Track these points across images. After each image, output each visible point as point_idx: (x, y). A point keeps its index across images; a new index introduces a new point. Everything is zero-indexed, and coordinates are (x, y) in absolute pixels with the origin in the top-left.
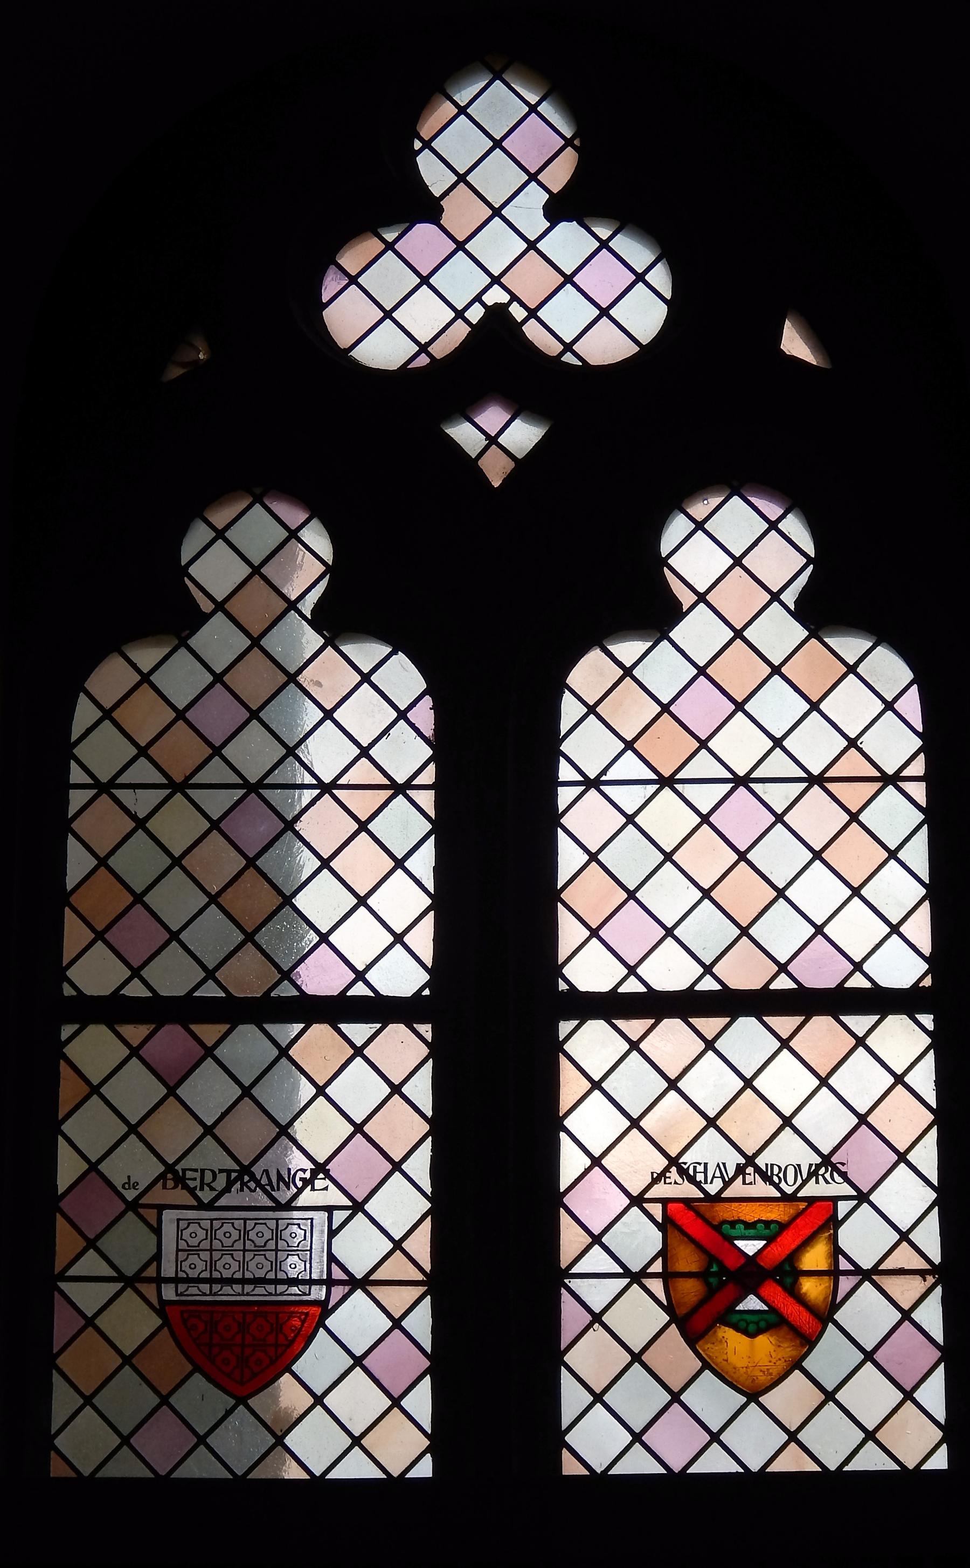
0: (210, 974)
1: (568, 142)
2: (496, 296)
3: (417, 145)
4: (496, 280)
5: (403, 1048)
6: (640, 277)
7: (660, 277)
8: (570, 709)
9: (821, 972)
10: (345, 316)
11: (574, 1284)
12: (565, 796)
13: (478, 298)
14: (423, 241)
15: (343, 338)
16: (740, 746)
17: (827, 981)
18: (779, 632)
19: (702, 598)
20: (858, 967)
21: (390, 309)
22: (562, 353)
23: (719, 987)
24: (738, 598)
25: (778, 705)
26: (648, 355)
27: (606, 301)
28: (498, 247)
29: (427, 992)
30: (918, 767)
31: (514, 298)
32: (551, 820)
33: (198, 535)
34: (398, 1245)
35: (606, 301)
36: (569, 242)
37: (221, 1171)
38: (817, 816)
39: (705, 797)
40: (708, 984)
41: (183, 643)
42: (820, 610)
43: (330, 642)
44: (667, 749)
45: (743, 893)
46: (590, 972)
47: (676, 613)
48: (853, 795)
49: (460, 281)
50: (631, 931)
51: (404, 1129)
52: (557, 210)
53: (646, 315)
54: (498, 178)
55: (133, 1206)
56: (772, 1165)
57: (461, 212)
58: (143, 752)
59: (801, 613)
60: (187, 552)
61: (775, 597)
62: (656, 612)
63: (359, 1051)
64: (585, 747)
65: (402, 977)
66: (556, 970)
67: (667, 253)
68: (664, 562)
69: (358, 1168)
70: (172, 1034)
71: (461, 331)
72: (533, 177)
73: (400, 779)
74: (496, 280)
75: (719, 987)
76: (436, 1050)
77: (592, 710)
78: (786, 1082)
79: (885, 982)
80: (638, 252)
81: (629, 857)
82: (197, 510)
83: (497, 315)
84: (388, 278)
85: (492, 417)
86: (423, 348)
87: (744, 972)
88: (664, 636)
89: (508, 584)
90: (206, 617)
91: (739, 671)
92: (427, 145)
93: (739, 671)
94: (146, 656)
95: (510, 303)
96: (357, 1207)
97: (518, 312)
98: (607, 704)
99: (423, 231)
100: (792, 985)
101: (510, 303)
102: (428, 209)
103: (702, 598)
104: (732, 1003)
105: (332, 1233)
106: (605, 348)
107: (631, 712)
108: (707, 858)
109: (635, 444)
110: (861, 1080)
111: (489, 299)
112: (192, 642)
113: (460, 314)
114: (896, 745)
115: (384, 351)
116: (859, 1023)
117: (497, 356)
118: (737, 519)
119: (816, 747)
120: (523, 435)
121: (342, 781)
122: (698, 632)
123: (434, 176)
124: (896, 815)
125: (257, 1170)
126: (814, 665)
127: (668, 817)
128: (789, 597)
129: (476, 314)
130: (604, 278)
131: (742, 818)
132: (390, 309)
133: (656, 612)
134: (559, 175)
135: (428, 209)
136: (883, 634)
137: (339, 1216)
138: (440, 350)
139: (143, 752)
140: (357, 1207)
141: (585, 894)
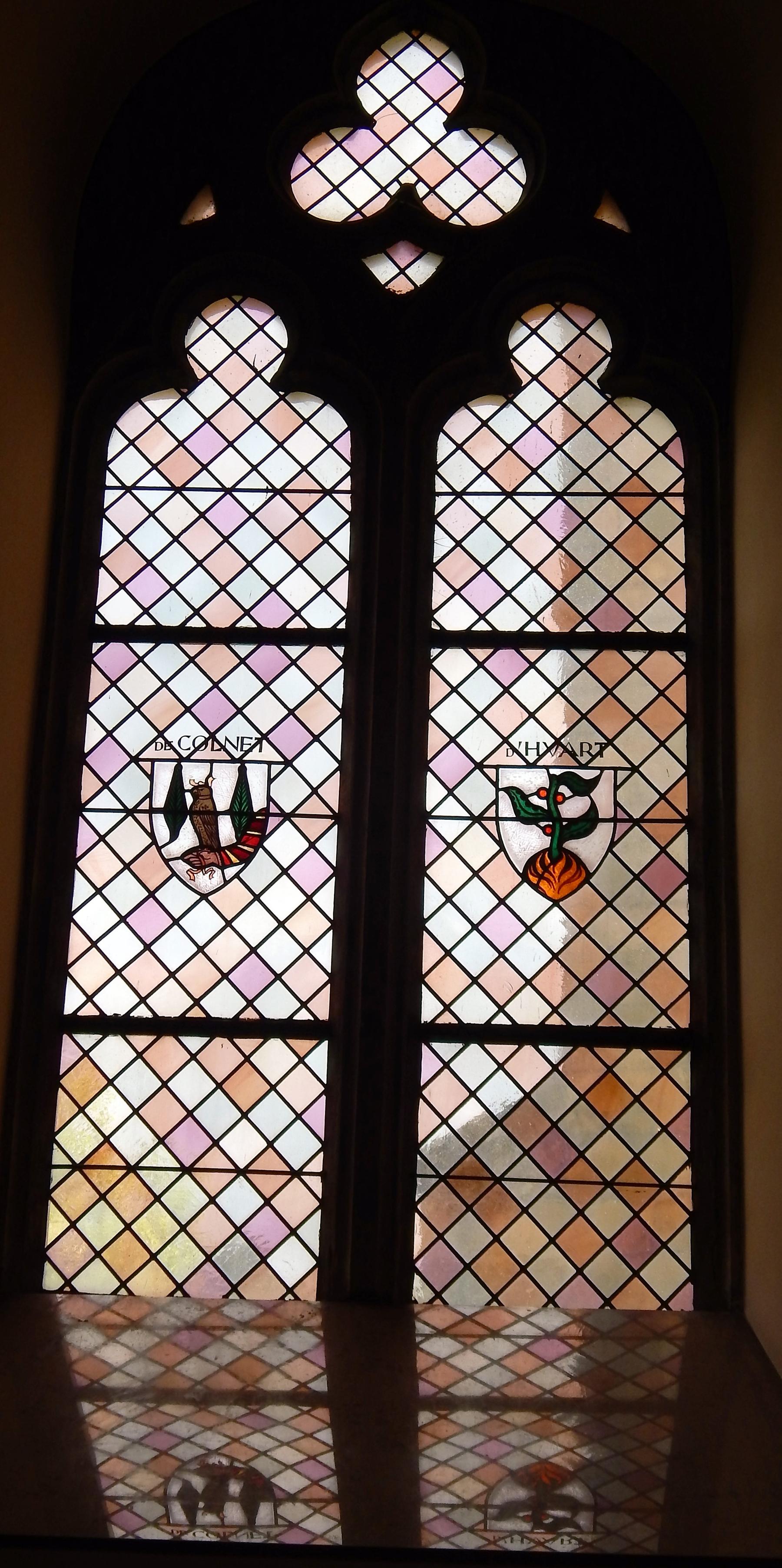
0: (197, 612)
1: (460, 82)
2: (409, 178)
3: (360, 80)
4: (409, 167)
5: (324, 661)
6: (505, 169)
7: (519, 170)
8: (444, 447)
9: (271, 616)
10: (306, 189)
11: (87, 814)
12: (110, 496)
13: (396, 179)
14: (363, 142)
15: (304, 204)
16: (229, 468)
17: (615, 627)
18: (260, 396)
19: (210, 374)
20: (298, 613)
21: (334, 184)
22: (450, 217)
23: (204, 625)
24: (234, 374)
25: (256, 444)
26: (508, 221)
27: (482, 184)
28: (411, 146)
29: (342, 626)
30: (347, 485)
31: (420, 179)
32: (100, 513)
33: (199, 327)
34: (315, 791)
35: (482, 184)
36: (459, 145)
37: (596, 744)
38: (279, 514)
39: (203, 501)
40: (482, 626)
41: (184, 397)
42: (285, 384)
43: (610, 402)
44: (180, 469)
45: (225, 564)
46: (453, 617)
47: (196, 383)
48: (302, 501)
49: (385, 168)
50: (483, 592)
51: (324, 714)
52: (451, 125)
53: (508, 193)
54: (413, 103)
55: (135, 759)
56: (243, 738)
57: (387, 124)
58: (484, 471)
59: (275, 384)
60: (189, 339)
61: (258, 374)
62: (182, 380)
63: (294, 662)
64: (455, 471)
65: (326, 615)
66: (94, 610)
67: (523, 153)
68: (187, 351)
69: (290, 737)
70: (269, 652)
71: (383, 201)
72: (436, 103)
73: (328, 487)
74: (409, 167)
75: (204, 625)
76: (688, 670)
77: (459, 447)
78: (242, 685)
79: (164, 622)
80: (504, 154)
81: (483, 544)
82: (196, 312)
83: (408, 191)
84: (337, 165)
85: (403, 255)
86: (358, 211)
87: (221, 615)
88: (510, 401)
89: (391, 363)
90: (198, 382)
91: (232, 421)
92: (367, 80)
93: (232, 421)
94: (484, 409)
95: (417, 183)
96: (288, 763)
97: (422, 190)
98: (470, 444)
99: (363, 134)
100: (304, 626)
101: (417, 183)
102: (368, 122)
103: (535, 378)
104: (210, 636)
105: (270, 781)
106: (480, 214)
107: (158, 445)
108: (202, 540)
109: (492, 278)
110: (292, 686)
111: (403, 179)
112: (191, 397)
113: (384, 189)
114: (333, 470)
115: (333, 210)
116: (532, 654)
117: (404, 218)
118: (236, 323)
119: (279, 470)
120: (423, 271)
121: (620, 491)
122: (207, 396)
123: (368, 99)
124: (331, 516)
125: (220, 736)
126: (281, 419)
127: (177, 513)
128: (594, 377)
129: (394, 189)
130: (481, 168)
131: (227, 515)
132: (334, 184)
133: (182, 380)
134: (451, 102)
135: (368, 122)
136: (330, 399)
137: (276, 769)
138: (369, 211)
139: (484, 471)
140: (288, 763)
141: (453, 568)
